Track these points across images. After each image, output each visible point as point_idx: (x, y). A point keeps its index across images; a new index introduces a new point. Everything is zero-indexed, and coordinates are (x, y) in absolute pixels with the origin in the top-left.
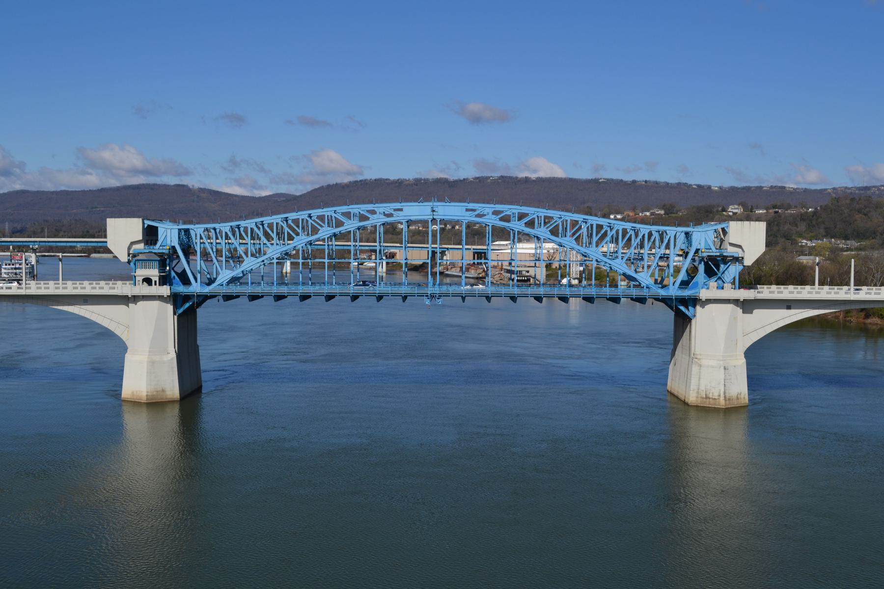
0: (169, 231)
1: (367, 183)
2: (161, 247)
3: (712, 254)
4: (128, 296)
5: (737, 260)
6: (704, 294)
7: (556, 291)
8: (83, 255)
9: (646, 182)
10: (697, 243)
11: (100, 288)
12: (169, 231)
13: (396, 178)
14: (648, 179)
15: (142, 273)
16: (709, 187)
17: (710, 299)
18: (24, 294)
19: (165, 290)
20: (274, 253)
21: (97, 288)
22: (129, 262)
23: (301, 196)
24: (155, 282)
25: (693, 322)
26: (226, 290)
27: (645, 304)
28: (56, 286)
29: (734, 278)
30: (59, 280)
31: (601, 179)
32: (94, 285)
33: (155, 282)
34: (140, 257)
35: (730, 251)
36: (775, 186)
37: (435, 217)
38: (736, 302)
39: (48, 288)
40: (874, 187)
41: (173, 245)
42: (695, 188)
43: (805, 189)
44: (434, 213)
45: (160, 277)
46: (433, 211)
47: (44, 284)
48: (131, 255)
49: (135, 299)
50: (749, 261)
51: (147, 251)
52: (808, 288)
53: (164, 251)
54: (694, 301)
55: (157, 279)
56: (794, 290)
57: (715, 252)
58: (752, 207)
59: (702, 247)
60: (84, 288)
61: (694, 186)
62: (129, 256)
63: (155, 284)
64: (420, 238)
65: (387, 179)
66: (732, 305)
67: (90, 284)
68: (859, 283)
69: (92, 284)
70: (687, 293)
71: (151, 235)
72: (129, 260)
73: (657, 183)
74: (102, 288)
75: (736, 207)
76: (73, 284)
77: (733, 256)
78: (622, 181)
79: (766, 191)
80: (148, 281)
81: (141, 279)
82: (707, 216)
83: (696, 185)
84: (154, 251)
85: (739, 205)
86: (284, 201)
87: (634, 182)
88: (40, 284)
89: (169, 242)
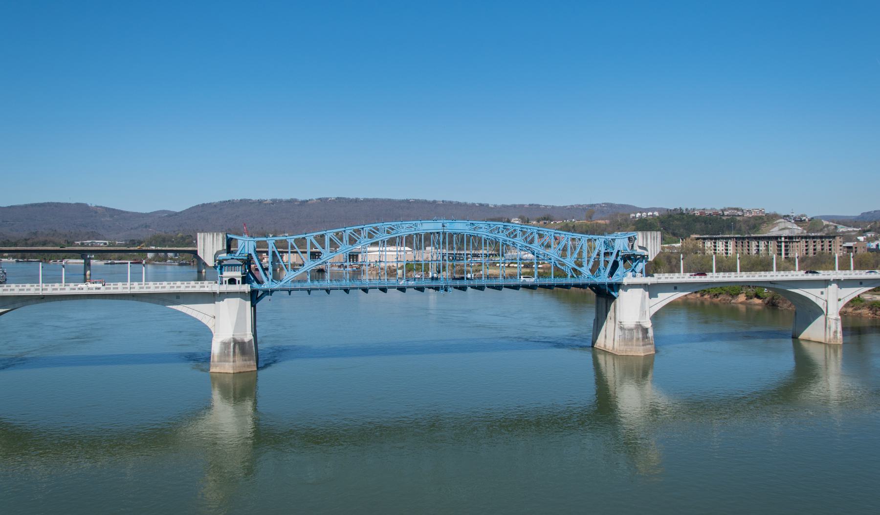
0: (247, 242)
1: (234, 203)
2: (240, 255)
3: (628, 253)
4: (245, 292)
5: (643, 257)
6: (626, 281)
7: (357, 284)
8: (36, 260)
9: (443, 201)
10: (618, 247)
11: (178, 287)
12: (247, 242)
13: (257, 198)
14: (444, 200)
15: (228, 274)
16: (488, 205)
17: (224, 293)
18: (129, 293)
19: (246, 288)
20: (328, 258)
21: (77, 289)
22: (215, 267)
23: (181, 212)
24: (239, 281)
25: (617, 300)
26: (290, 286)
27: (423, 292)
28: (140, 286)
29: (642, 269)
30: (142, 281)
31: (411, 199)
32: (158, 285)
33: (239, 281)
34: (225, 263)
35: (639, 251)
36: (532, 204)
37: (445, 230)
38: (645, 286)
39: (117, 288)
40: (597, 204)
41: (249, 253)
42: (477, 206)
43: (553, 206)
44: (444, 228)
45: (243, 278)
46: (444, 226)
47: (114, 285)
48: (217, 261)
49: (222, 296)
50: (651, 259)
51: (230, 257)
52: (677, 274)
53: (244, 258)
54: (617, 286)
55: (240, 279)
56: (181, 285)
57: (629, 252)
58: (528, 219)
59: (621, 249)
60: (150, 288)
61: (477, 205)
62: (215, 261)
63: (239, 283)
64: (498, 243)
65: (250, 200)
66: (239, 299)
67: (168, 284)
68: (68, 281)
69: (170, 284)
70: (614, 279)
71: (230, 246)
72: (215, 265)
73: (451, 202)
74: (13, 290)
75: (517, 219)
76: (123, 285)
77: (641, 255)
78: (426, 201)
79: (527, 208)
80: (232, 281)
81: (227, 279)
82: (619, 228)
83: (478, 204)
84: (235, 258)
85: (519, 218)
86: (167, 216)
87: (434, 202)
88: (110, 285)
89: (246, 251)
